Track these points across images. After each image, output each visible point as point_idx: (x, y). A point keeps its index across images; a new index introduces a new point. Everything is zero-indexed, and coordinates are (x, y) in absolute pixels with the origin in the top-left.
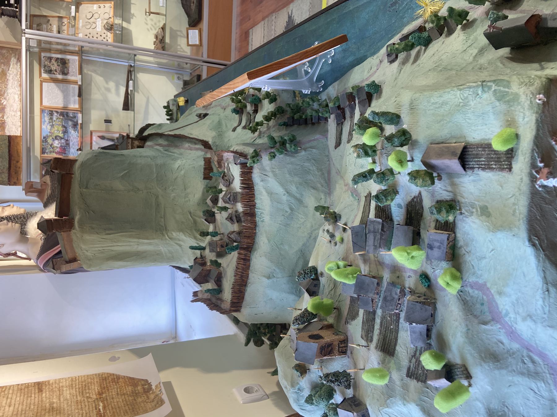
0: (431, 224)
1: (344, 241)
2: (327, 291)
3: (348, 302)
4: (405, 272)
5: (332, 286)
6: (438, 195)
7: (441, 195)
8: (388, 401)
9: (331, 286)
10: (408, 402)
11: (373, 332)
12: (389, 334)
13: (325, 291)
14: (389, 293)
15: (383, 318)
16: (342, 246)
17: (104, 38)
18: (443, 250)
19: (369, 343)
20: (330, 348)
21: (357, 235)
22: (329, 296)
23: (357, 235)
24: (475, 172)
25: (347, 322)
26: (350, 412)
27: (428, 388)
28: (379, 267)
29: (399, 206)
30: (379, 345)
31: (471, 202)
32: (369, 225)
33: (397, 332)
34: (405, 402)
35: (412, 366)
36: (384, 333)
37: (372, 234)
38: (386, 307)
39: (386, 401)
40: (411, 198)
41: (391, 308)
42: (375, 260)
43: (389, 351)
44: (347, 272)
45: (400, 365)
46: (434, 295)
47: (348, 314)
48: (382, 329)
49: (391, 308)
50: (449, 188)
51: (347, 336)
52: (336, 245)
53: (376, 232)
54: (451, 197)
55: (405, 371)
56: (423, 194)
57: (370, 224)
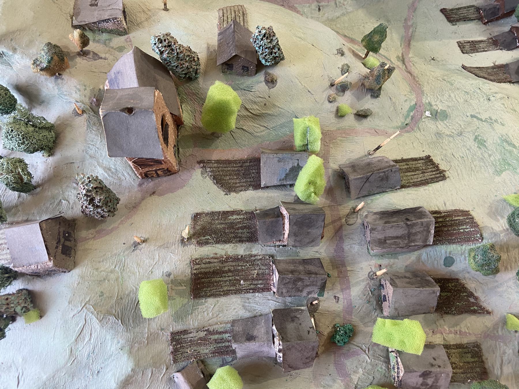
0: (439, 335)
1: (340, 120)
8: (112, 319)
9: (255, 107)
10: (130, 352)
11: (217, 242)
12: (227, 279)
15: (250, 260)
20: (152, 163)
21: (382, 180)
25: (203, 163)
26: (48, 254)
27: (167, 369)
30: (203, 266)
33: (238, 292)
34: (127, 348)
35: (191, 335)
36: (226, 269)
38: (284, 284)
39: (111, 314)
42: (340, 219)
45: (185, 316)
47: (218, 162)
48: (231, 263)
53: (409, 237)
55: (179, 327)
57: (424, 225)
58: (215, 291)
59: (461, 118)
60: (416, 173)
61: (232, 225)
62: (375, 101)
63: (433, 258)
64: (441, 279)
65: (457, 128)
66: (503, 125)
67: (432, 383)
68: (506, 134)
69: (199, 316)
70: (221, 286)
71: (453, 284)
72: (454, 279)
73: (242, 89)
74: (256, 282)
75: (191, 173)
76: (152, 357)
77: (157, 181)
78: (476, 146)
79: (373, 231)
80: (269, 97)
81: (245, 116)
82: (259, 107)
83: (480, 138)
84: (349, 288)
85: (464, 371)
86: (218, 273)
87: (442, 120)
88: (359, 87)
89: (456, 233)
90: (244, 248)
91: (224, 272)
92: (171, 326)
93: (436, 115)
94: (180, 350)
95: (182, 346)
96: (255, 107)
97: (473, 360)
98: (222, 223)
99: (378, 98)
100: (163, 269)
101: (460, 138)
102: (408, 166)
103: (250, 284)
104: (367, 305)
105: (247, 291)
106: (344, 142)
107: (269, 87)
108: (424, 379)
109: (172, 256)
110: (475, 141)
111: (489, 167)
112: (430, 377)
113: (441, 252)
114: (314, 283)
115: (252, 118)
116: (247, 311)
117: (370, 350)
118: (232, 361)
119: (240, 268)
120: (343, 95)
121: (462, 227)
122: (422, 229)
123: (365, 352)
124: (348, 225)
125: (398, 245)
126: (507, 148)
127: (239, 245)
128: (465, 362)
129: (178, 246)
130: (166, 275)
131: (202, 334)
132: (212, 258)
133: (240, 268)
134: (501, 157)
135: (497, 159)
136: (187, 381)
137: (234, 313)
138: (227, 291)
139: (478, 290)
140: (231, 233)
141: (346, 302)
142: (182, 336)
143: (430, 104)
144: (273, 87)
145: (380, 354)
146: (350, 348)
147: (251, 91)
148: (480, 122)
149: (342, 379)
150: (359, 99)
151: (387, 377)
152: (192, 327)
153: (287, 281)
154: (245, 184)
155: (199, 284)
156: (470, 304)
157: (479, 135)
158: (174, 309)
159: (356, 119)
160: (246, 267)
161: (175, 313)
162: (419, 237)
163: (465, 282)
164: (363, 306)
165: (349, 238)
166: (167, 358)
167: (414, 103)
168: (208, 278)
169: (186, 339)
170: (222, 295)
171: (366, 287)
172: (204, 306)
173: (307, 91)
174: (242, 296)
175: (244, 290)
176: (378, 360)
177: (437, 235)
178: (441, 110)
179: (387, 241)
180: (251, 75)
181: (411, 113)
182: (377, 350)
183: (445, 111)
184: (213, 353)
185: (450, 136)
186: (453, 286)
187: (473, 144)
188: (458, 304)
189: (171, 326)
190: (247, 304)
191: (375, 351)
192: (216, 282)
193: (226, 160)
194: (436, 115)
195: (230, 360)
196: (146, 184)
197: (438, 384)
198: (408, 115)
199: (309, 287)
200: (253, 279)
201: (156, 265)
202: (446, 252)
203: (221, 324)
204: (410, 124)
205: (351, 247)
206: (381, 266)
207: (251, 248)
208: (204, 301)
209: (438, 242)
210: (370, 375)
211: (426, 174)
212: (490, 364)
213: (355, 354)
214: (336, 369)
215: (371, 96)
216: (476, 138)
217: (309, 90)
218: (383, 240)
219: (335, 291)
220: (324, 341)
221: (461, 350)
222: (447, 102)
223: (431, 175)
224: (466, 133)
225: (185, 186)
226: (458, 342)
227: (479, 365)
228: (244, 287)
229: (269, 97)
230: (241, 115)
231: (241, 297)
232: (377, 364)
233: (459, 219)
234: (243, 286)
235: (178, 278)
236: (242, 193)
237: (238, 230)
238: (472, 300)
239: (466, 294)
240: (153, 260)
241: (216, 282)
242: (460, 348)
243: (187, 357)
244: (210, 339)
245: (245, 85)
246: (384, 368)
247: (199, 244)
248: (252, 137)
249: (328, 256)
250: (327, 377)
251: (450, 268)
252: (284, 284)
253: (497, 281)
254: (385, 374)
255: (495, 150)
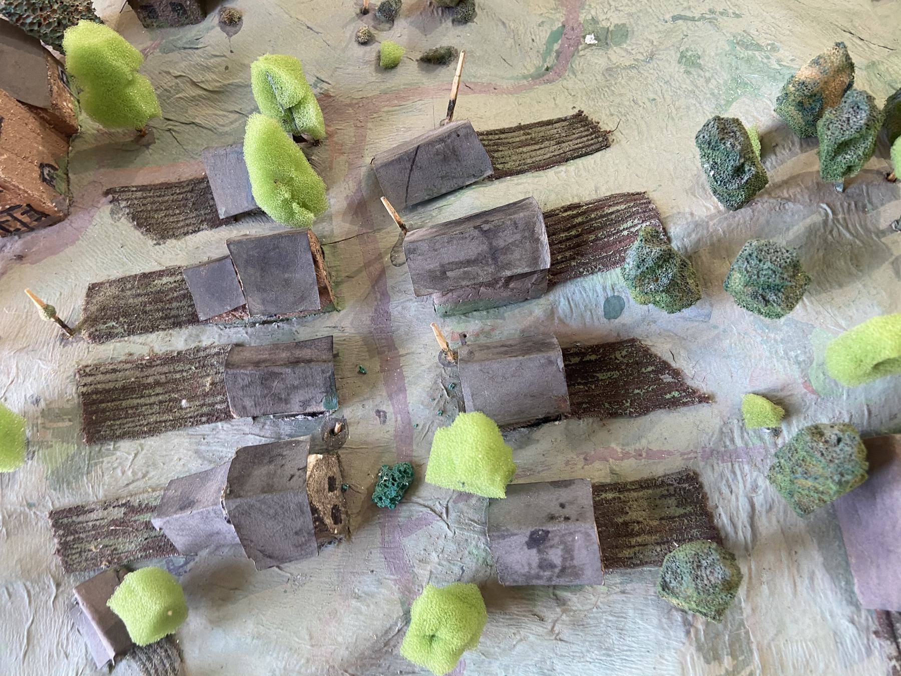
0: (597, 465)
1: (388, 75)
2: (181, 64)
3: (187, 171)
4: (390, 397)
5: (212, 80)
6: (722, 475)
7: (725, 491)
9: (209, 76)
11: (131, 332)
12: (153, 399)
13: (174, 56)
14: (296, 383)
16: (370, 74)
17: (32, 162)
18: (538, 577)
19: (84, 334)
21: (445, 159)
22: (168, 82)
23: (445, 159)
24: (877, 642)
25: (113, 194)
27: (58, 585)
28: (363, 280)
29: (614, 307)
30: (100, 377)
31: (747, 633)
32: (516, 225)
33: (178, 423)
35: (93, 516)
36: (151, 380)
37: (485, 247)
40: (667, 357)
41: (248, 403)
42: (380, 256)
43: (96, 422)
44: (293, 174)
45: (76, 478)
46: (360, 527)
47: (143, 188)
48: (160, 369)
49: (248, 403)
50: (767, 526)
51: (66, 215)
52: (364, 43)
53: (495, 259)
54: (729, 529)
55: (66, 500)
56: (703, 411)
57: (521, 225)
58: (130, 425)
59: (654, 29)
60: (542, 146)
61: (159, 297)
62: (461, 30)
63: (581, 305)
64: (597, 346)
65: (646, 49)
66: (738, 16)
67: (560, 559)
68: (744, 31)
69: (106, 477)
70: (144, 415)
71: (624, 353)
72: (627, 341)
73: (180, 49)
74: (209, 400)
75: (91, 213)
76: (20, 560)
77: (28, 237)
78: (682, 70)
79: (411, 256)
80: (232, 52)
81: (194, 97)
82: (216, 75)
83: (689, 53)
84: (402, 390)
85: (662, 537)
86: (133, 390)
87: (618, 44)
88: (424, 9)
89: (614, 242)
90: (184, 337)
91: (146, 386)
92: (47, 498)
93: (605, 38)
94: (75, 546)
95: (79, 538)
96: (209, 76)
97: (681, 511)
98: (139, 295)
99: (469, 24)
100: (25, 391)
101: (651, 66)
102: (529, 137)
103: (202, 406)
104: (441, 418)
105: (196, 421)
106: (396, 114)
107: (228, 34)
108: (539, 551)
109: (41, 365)
110: (679, 62)
111: (705, 102)
112: (551, 547)
113: (594, 290)
114: (310, 381)
115: (209, 99)
116: (206, 462)
117: (451, 511)
118: (186, 563)
119: (178, 376)
120: (390, 28)
121: (625, 226)
122: (518, 236)
123: (440, 516)
124: (395, 265)
125: (474, 278)
126: (742, 55)
127: (174, 332)
128: (661, 519)
129: (54, 346)
130: (33, 403)
131: (118, 513)
132: (126, 362)
133: (178, 376)
134: (729, 76)
135: (721, 82)
136: (87, 604)
137: (179, 468)
138: (156, 422)
139: (679, 353)
140: (158, 310)
141: (399, 419)
142: (74, 518)
143: (594, 21)
144: (236, 33)
145: (472, 518)
146: (410, 511)
147: (197, 48)
148: (690, 23)
149: (395, 577)
150: (425, 31)
151: (491, 566)
152: (92, 499)
153: (246, 382)
154: (193, 221)
155: (95, 413)
156: (663, 388)
157: (687, 50)
158: (50, 465)
159: (423, 70)
160: (191, 372)
161: (53, 472)
162: (517, 255)
163: (650, 344)
164: (433, 422)
165: (399, 291)
166: (52, 561)
167: (560, 25)
168: (113, 401)
169: (85, 525)
170: (146, 432)
171: (435, 383)
172: (114, 458)
173: (305, 28)
174: (191, 431)
175: (191, 417)
176: (468, 530)
177: (578, 254)
178: (616, 26)
179: (449, 274)
180: (197, 21)
181: (556, 44)
182: (465, 509)
183: (624, 25)
184: (145, 550)
185: (631, 67)
186: (624, 357)
187: (677, 69)
188: (637, 391)
189: (47, 498)
190: (203, 448)
191: (462, 512)
192: (132, 408)
193: (162, 184)
194: (606, 39)
195: (182, 563)
196: (9, 246)
197: (575, 563)
198: (548, 51)
199: (301, 392)
200: (206, 395)
201: (12, 385)
202: (604, 288)
203: (154, 490)
204: (555, 68)
205: (403, 308)
206: (465, 336)
207: (198, 336)
208: (111, 447)
209: (581, 270)
210: (454, 564)
211: (563, 145)
212: (725, 519)
213: (421, 523)
214: (384, 560)
215: (453, 21)
216: (683, 55)
217: (309, 26)
218: (438, 273)
219: (378, 400)
220: (360, 505)
221: (650, 491)
222: (627, 8)
223: (577, 144)
224: (661, 52)
225: (78, 239)
226: (645, 474)
227: (696, 521)
228: (190, 412)
229: (232, 52)
230: (187, 97)
231: (188, 434)
232: (467, 540)
233: (618, 211)
234: (188, 410)
235: (53, 406)
236: (188, 237)
237: (170, 303)
238: (667, 378)
239: (653, 368)
240: (6, 376)
241: (132, 408)
242: (648, 487)
243: (92, 559)
244: (135, 521)
245: (184, 40)
246: (483, 546)
247: (94, 339)
248: (215, 136)
249: (359, 333)
250: (365, 578)
251: (617, 321)
252: (243, 388)
253: (716, 327)
254: (485, 560)
255: (718, 67)
